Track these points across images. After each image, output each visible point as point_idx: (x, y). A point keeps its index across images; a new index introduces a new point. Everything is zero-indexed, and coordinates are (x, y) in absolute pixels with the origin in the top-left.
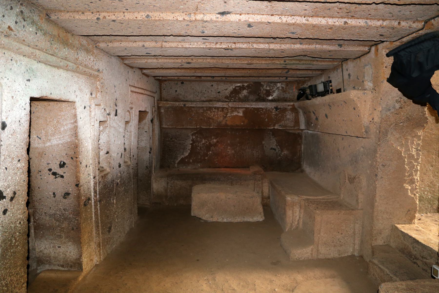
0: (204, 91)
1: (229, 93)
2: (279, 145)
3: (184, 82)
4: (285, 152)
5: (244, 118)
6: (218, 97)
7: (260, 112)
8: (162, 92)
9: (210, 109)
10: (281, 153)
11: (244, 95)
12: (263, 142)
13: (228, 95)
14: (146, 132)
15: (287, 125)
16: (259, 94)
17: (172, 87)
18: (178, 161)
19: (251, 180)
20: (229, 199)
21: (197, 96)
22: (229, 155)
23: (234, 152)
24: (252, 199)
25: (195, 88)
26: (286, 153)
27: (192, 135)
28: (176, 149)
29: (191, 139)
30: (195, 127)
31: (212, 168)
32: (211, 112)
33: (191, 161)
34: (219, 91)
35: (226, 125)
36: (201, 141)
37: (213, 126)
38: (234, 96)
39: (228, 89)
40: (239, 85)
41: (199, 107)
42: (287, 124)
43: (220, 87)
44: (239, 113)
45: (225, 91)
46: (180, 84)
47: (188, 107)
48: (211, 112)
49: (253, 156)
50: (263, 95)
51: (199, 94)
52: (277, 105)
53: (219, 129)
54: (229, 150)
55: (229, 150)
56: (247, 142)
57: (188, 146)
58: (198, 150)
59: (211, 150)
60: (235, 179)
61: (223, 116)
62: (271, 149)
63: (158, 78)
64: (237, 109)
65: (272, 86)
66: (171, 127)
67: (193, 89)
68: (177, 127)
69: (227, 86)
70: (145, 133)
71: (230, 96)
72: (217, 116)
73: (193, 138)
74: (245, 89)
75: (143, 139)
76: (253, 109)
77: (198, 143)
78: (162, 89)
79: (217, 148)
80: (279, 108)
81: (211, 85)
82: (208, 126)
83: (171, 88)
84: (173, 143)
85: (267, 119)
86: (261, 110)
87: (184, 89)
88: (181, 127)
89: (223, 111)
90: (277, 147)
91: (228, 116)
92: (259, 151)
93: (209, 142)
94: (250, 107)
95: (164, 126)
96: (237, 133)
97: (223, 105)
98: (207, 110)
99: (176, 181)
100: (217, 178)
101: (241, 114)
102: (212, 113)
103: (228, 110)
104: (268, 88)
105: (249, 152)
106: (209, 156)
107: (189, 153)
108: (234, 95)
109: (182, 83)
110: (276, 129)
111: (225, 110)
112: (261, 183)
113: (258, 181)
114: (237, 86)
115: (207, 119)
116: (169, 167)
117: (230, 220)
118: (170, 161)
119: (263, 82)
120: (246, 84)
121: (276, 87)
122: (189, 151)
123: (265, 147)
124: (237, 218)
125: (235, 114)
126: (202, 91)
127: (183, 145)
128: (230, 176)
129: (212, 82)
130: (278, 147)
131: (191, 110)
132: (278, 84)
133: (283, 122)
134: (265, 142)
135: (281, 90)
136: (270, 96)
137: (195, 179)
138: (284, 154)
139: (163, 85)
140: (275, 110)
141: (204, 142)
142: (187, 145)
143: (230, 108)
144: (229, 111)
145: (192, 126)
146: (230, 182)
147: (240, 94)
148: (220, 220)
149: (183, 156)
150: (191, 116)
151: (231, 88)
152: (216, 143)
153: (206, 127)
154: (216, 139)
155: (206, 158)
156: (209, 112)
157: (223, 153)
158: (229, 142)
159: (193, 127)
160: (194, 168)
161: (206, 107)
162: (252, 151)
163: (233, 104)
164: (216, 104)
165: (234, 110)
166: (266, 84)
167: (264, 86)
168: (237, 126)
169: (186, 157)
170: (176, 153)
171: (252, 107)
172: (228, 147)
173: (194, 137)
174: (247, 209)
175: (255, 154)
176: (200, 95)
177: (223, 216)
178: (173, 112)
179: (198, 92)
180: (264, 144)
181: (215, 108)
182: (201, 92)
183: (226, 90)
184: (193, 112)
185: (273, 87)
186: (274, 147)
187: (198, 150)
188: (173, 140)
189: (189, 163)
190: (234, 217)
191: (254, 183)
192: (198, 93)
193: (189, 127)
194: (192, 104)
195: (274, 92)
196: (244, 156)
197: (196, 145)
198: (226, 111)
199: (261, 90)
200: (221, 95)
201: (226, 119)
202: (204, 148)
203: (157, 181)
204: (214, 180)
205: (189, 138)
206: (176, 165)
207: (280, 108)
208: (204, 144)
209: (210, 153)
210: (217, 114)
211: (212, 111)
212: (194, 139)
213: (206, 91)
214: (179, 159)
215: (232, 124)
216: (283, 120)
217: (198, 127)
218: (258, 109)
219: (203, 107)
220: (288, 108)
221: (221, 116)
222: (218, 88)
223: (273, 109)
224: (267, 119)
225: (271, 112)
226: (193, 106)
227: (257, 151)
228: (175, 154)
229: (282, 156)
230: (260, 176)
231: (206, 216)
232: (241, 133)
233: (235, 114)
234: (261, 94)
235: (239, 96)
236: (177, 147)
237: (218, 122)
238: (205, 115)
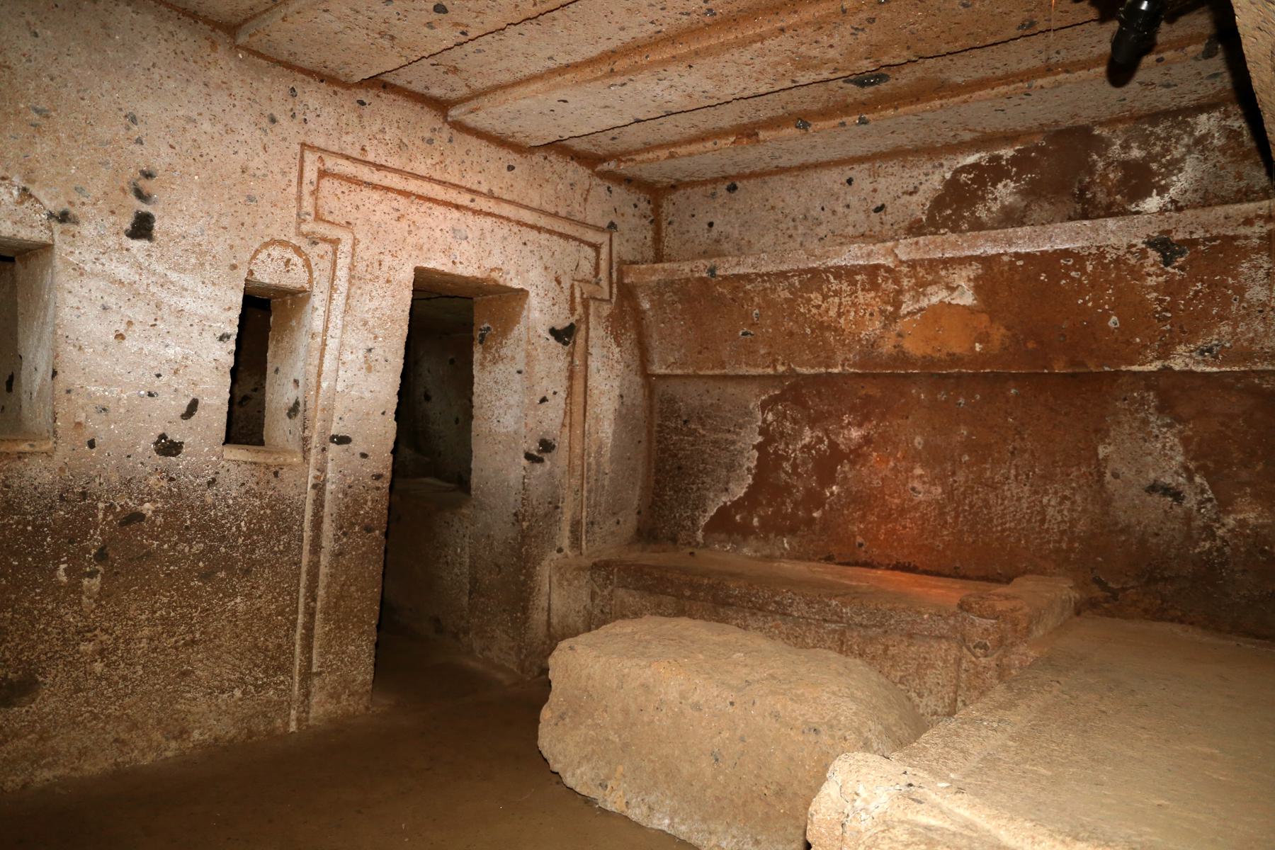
0: (816, 212)
1: (928, 204)
2: (1201, 469)
3: (738, 184)
4: (1251, 516)
5: (985, 318)
6: (877, 228)
7: (1067, 276)
8: (664, 235)
9: (815, 278)
10: (1217, 520)
11: (1003, 207)
12: (1102, 451)
13: (924, 218)
14: (519, 372)
15: (1257, 347)
16: (1083, 191)
17: (694, 213)
18: (707, 519)
19: (940, 638)
20: (697, 707)
21: (790, 236)
22: (916, 508)
23: (943, 492)
24: (812, 737)
25: (782, 204)
26: (1252, 521)
27: (764, 407)
28: (701, 467)
29: (759, 423)
30: (770, 371)
31: (840, 564)
32: (825, 297)
33: (756, 521)
34: (879, 204)
35: (901, 358)
36: (798, 435)
37: (843, 365)
38: (950, 215)
39: (922, 188)
40: (971, 159)
41: (768, 274)
42: (1252, 340)
43: (882, 183)
44: (956, 293)
45: (907, 197)
46: (726, 192)
47: (725, 278)
48: (825, 297)
49: (1043, 521)
50: (1109, 194)
51: (796, 228)
52: (1166, 227)
53: (874, 376)
54: (916, 484)
55: (916, 484)
56: (1010, 448)
57: (747, 455)
58: (783, 475)
59: (839, 477)
60: (857, 619)
61: (882, 312)
62: (1153, 488)
63: (612, 165)
64: (943, 273)
65: (1158, 138)
66: (679, 372)
67: (773, 208)
68: (701, 369)
69: (915, 173)
70: (518, 376)
71: (931, 217)
72: (853, 314)
73: (764, 421)
74: (1007, 175)
75: (512, 402)
76: (1020, 263)
77: (787, 445)
78: (664, 225)
79: (864, 471)
80: (1184, 242)
81: (844, 180)
82: (820, 366)
83: (693, 216)
84: (690, 439)
85: (1114, 318)
86: (1073, 268)
87: (737, 212)
88: (717, 372)
89: (874, 286)
90: (1190, 479)
91: (904, 309)
92: (1078, 498)
93: (828, 437)
94: (1006, 254)
95: (658, 369)
96: (962, 400)
97: (869, 255)
98: (806, 286)
99: (621, 592)
100: (776, 602)
101: (966, 298)
102: (830, 300)
103: (897, 281)
104: (1136, 153)
105: (1019, 499)
106: (827, 507)
107: (750, 487)
108: (949, 212)
109: (732, 188)
110: (1182, 372)
111: (885, 280)
112: (993, 664)
113: (979, 652)
114: (964, 167)
115: (813, 331)
116: (674, 540)
117: (683, 828)
118: (681, 515)
119: (1101, 124)
120: (1007, 153)
121: (1186, 140)
122: (750, 480)
123: (1115, 475)
124: (720, 829)
125: (937, 296)
126: (808, 210)
127: (726, 449)
128: (834, 603)
129: (846, 168)
130: (1198, 479)
131: (741, 295)
132: (1204, 117)
133: (1225, 328)
134: (1111, 449)
135: (1223, 150)
136: (1151, 196)
137: (688, 593)
138: (1243, 524)
139: (667, 207)
140: (1154, 255)
141: (807, 440)
142: (741, 452)
143: (905, 269)
144: (905, 282)
145: (756, 366)
146: (835, 631)
147: (980, 206)
148: (636, 814)
149: (725, 499)
150: (751, 322)
151: (933, 179)
152: (860, 446)
153: (813, 368)
154: (860, 425)
155: (815, 515)
156: (816, 298)
157: (890, 495)
158: (918, 441)
159: (760, 371)
160: (764, 553)
161: (800, 273)
162: (1036, 492)
163: (917, 243)
164: (837, 254)
165: (930, 278)
166: (1126, 131)
167: (1109, 144)
168: (954, 360)
169: (737, 505)
170: (703, 483)
171: (1013, 250)
172: (913, 468)
173: (770, 417)
174: (780, 793)
175: (1050, 511)
176: (801, 230)
177: (652, 799)
178: (680, 306)
179: (794, 220)
180: (1106, 459)
181: (839, 272)
182: (805, 218)
183: (911, 194)
184: (752, 299)
185: (1167, 139)
186: (1167, 480)
187: (783, 475)
188: (693, 427)
189: (745, 531)
190: (704, 820)
191: (958, 661)
192: (791, 224)
193: (744, 370)
194: (738, 264)
195: (1175, 166)
196: (991, 520)
197: (776, 452)
198: (891, 286)
199: (1091, 170)
200: (888, 219)
201: (898, 327)
202: (810, 466)
203: (566, 583)
204: (760, 610)
205: (750, 423)
206: (700, 534)
207: (1192, 243)
208: (807, 447)
209: (832, 494)
210: (854, 304)
211: (829, 289)
212: (771, 423)
213: (823, 209)
214: (712, 511)
215: (929, 351)
216: (1221, 318)
217: (781, 369)
218: (1049, 261)
219: (783, 275)
220: (1246, 237)
221: (871, 314)
222: (875, 190)
223: (1143, 252)
224: (1114, 318)
225: (1137, 273)
226: (741, 270)
227: (1065, 498)
228: (698, 489)
229: (1222, 538)
230: (988, 623)
231: (583, 769)
232: (978, 397)
233: (937, 296)
234: (1094, 189)
235: (973, 213)
236: (706, 456)
237: (862, 346)
238: (802, 310)
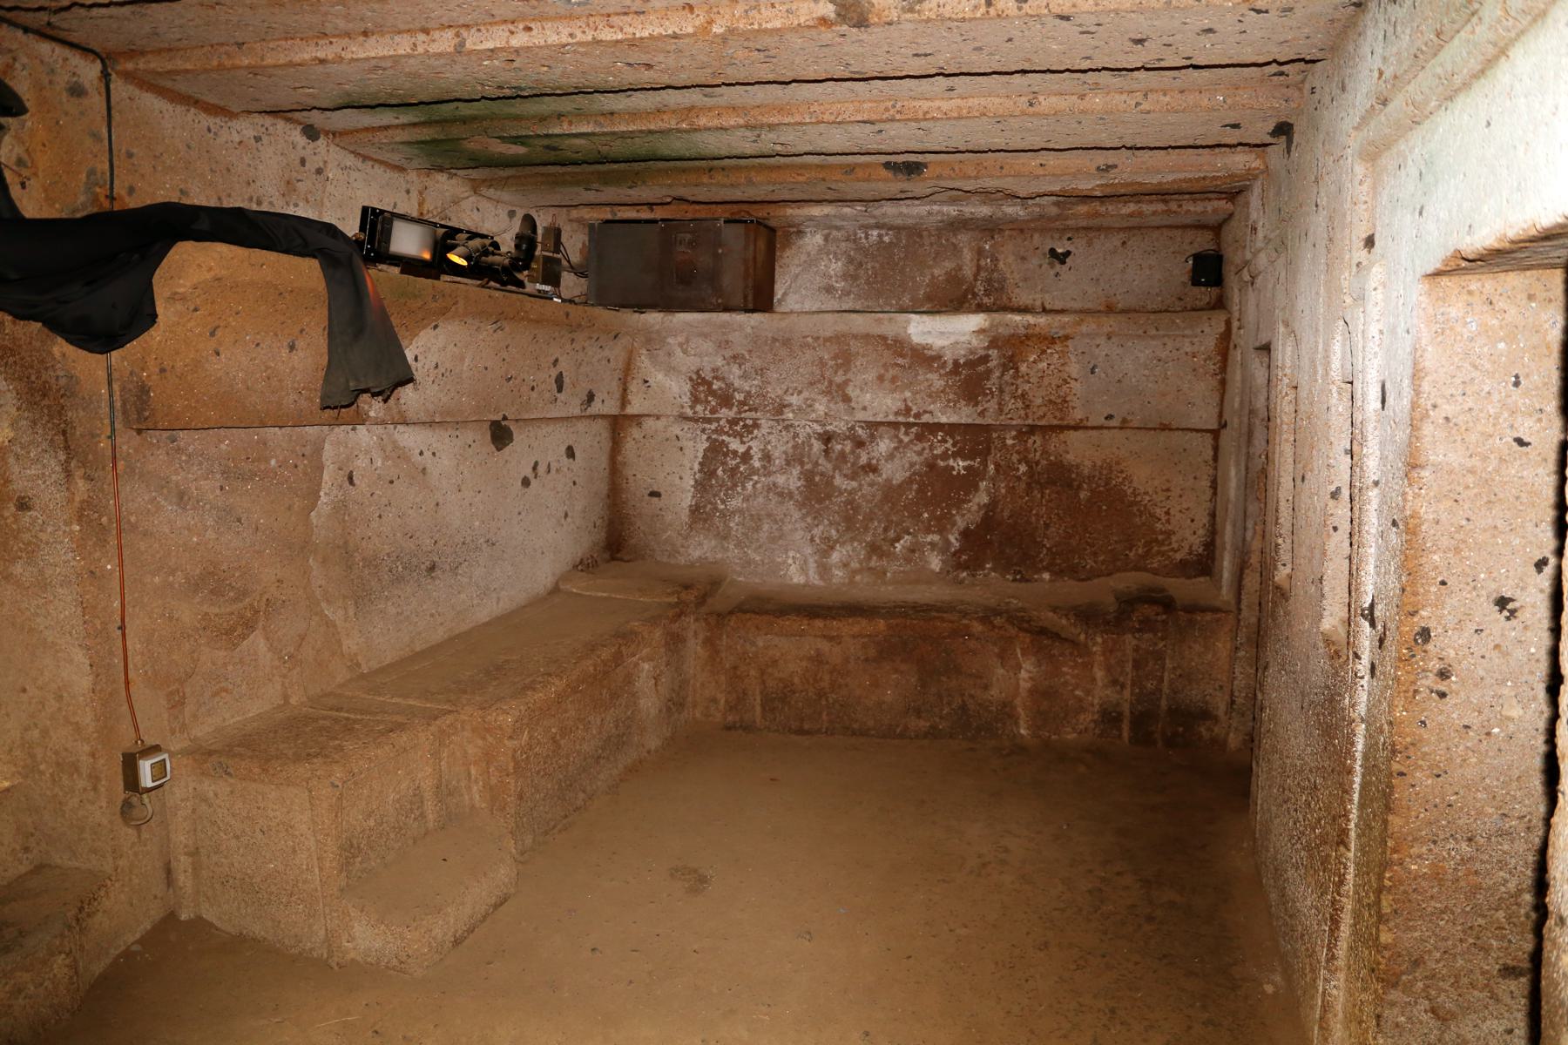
209: (1095, 644)
